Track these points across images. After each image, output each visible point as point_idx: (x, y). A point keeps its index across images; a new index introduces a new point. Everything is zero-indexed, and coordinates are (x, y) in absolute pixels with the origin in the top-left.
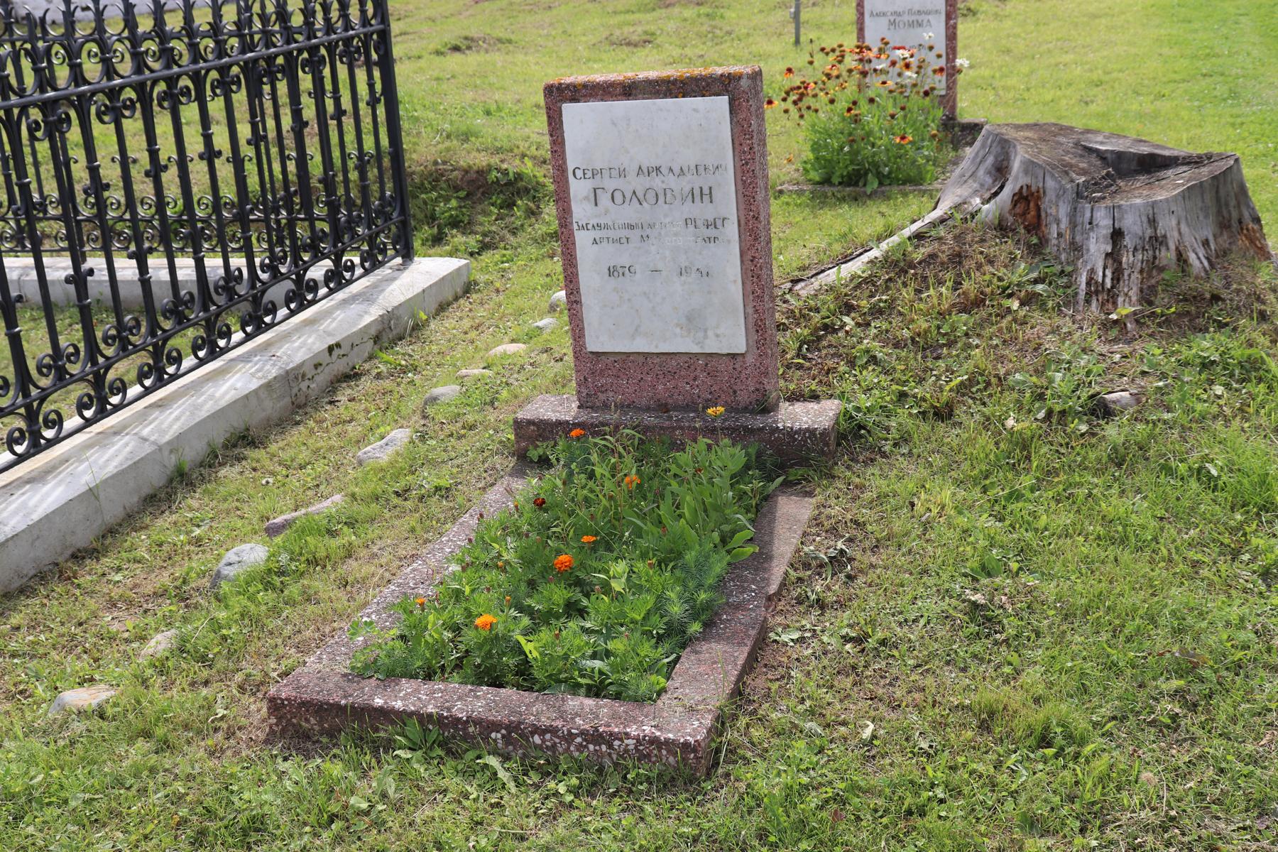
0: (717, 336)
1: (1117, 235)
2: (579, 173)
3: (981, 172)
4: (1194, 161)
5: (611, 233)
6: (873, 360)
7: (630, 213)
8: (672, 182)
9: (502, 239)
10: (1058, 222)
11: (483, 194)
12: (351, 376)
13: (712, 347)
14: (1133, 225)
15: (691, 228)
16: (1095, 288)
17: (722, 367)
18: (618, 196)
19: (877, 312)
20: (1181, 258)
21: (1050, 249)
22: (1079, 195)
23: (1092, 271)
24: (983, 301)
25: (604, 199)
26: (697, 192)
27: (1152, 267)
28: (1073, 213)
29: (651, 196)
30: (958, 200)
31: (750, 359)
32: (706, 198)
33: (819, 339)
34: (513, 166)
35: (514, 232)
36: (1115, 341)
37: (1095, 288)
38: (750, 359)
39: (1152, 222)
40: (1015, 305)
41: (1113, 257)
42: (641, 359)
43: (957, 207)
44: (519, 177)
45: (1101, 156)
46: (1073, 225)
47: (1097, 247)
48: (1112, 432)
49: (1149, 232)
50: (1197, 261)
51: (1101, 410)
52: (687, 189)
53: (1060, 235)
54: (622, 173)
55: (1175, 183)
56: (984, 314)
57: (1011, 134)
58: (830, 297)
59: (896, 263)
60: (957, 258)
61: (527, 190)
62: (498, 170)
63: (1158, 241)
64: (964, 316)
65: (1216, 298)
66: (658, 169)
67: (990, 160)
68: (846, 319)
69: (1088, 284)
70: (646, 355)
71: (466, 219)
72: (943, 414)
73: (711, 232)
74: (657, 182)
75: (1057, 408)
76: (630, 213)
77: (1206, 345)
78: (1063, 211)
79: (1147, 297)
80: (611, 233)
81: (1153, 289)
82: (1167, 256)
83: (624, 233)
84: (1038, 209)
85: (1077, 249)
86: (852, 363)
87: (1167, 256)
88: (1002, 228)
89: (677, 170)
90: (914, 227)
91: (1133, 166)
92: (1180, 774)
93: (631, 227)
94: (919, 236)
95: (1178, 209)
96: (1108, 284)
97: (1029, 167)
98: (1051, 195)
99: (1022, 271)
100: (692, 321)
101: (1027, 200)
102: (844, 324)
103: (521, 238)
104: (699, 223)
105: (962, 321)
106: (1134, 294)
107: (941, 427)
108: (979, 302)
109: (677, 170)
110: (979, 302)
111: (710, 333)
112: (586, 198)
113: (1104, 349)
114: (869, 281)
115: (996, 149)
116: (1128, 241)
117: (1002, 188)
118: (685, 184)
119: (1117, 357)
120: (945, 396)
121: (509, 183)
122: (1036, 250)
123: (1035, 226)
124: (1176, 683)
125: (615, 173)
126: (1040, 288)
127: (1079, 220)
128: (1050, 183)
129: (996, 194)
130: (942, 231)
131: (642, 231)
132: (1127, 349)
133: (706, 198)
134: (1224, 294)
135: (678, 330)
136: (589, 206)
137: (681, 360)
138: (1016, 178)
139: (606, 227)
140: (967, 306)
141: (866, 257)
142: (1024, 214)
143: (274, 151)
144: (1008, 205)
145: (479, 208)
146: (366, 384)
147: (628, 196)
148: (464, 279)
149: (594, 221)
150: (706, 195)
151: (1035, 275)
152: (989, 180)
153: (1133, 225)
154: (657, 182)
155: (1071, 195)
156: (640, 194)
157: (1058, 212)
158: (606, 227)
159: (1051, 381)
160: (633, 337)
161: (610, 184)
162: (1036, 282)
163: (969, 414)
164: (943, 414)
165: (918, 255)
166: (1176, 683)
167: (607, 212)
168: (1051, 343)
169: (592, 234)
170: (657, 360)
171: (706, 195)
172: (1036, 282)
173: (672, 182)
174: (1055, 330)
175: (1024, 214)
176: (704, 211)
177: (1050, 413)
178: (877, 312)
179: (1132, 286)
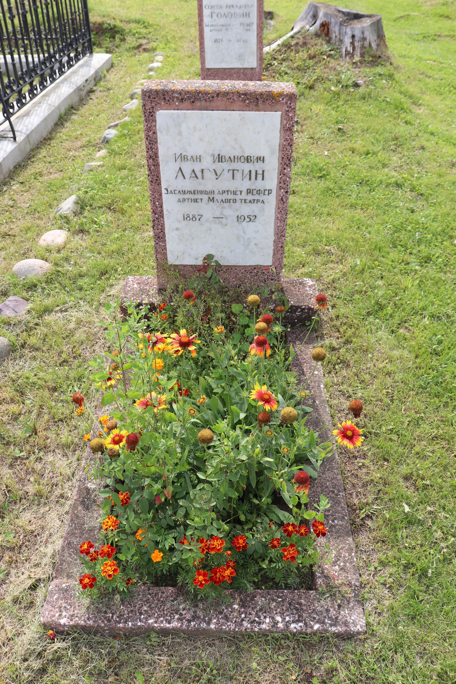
0: (248, 62)
1: (353, 36)
2: (207, 7)
3: (308, 17)
4: (370, 16)
5: (216, 28)
6: (286, 73)
7: (222, 21)
8: (237, 10)
9: (114, 50)
10: (335, 33)
11: (102, 33)
12: (91, 91)
13: (246, 66)
14: (358, 34)
15: (242, 26)
16: (347, 53)
17: (248, 72)
18: (219, 16)
19: (284, 60)
20: (370, 45)
21: (333, 41)
22: (341, 24)
23: (346, 48)
24: (315, 56)
25: (215, 16)
26: (245, 14)
27: (363, 47)
28: (340, 30)
29: (230, 15)
30: (302, 26)
31: (257, 70)
32: (247, 16)
33: (268, 68)
34: (112, 23)
35: (117, 47)
36: (355, 68)
37: (347, 53)
38: (257, 70)
39: (363, 33)
40: (325, 57)
41: (352, 43)
42: (223, 70)
43: (302, 28)
44: (115, 26)
45: (343, 13)
46: (340, 34)
47: (347, 40)
48: (361, 90)
49: (362, 36)
50: (374, 45)
51: (356, 85)
52: (242, 13)
53: (336, 37)
54: (221, 7)
55: (367, 22)
56: (317, 60)
57: (319, 5)
58: (269, 55)
59: (286, 46)
60: (305, 44)
61: (119, 32)
62: (107, 23)
63: (364, 39)
64: (311, 61)
65: (380, 57)
66: (233, 6)
67: (311, 13)
68: (275, 62)
69: (346, 51)
70: (225, 69)
71: (98, 43)
72: (311, 87)
73: (248, 28)
74: (232, 10)
75: (345, 85)
76: (222, 21)
77: (379, 70)
78: (337, 29)
79: (362, 55)
80: (216, 28)
81: (364, 53)
82: (366, 44)
83: (221, 28)
84: (328, 29)
85: (341, 41)
86: (280, 74)
87: (366, 44)
88: (317, 35)
89: (239, 6)
90: (291, 33)
91: (352, 17)
92: (401, 159)
93: (223, 26)
94: (292, 37)
95: (369, 28)
96: (351, 52)
97: (326, 15)
98: (333, 24)
99: (326, 48)
100: (240, 57)
101: (325, 26)
102: (274, 64)
103: (121, 49)
104: (245, 24)
105: (311, 62)
106: (359, 54)
107: (312, 91)
108: (314, 57)
109: (239, 6)
110: (314, 57)
111: (246, 61)
112: (209, 16)
113: (353, 70)
114: (279, 51)
115: (313, 9)
116: (357, 39)
117: (315, 22)
118: (240, 11)
119: (357, 72)
120: (311, 82)
121: (111, 29)
122: (328, 42)
123: (327, 34)
124: (394, 143)
125: (219, 7)
126: (332, 52)
127: (341, 32)
128: (333, 20)
129: (313, 24)
130: (298, 36)
131: (226, 27)
132: (359, 70)
133: (247, 16)
134: (382, 56)
135: (236, 60)
136: (209, 19)
137: (236, 70)
138: (321, 19)
139: (215, 26)
140: (311, 57)
141: (276, 44)
142: (323, 30)
143: (15, 12)
144: (318, 27)
145: (102, 38)
146: (98, 94)
147: (223, 14)
148: (110, 62)
149: (211, 24)
150: (247, 15)
151: (330, 49)
152: (311, 20)
153: (358, 34)
154: (232, 10)
155: (339, 24)
156: (226, 14)
157: (335, 30)
158: (215, 26)
159: (341, 77)
160: (221, 63)
161: (217, 11)
162: (330, 51)
163: (319, 87)
164: (311, 87)
165: (293, 43)
166: (394, 143)
167: (215, 20)
168: (339, 68)
169: (209, 28)
170: (228, 71)
171: (247, 15)
172: (330, 51)
173: (237, 10)
174: (339, 64)
175: (323, 30)
176: (246, 20)
177: (342, 87)
178: (284, 60)
179: (358, 52)
